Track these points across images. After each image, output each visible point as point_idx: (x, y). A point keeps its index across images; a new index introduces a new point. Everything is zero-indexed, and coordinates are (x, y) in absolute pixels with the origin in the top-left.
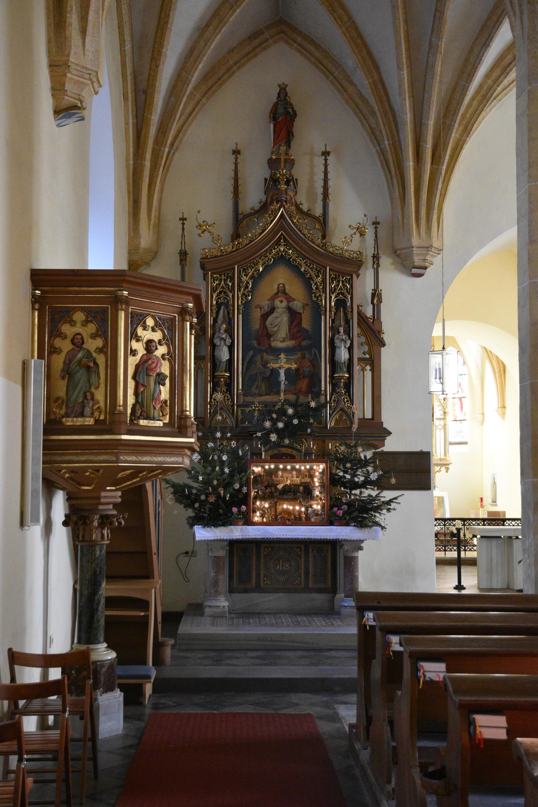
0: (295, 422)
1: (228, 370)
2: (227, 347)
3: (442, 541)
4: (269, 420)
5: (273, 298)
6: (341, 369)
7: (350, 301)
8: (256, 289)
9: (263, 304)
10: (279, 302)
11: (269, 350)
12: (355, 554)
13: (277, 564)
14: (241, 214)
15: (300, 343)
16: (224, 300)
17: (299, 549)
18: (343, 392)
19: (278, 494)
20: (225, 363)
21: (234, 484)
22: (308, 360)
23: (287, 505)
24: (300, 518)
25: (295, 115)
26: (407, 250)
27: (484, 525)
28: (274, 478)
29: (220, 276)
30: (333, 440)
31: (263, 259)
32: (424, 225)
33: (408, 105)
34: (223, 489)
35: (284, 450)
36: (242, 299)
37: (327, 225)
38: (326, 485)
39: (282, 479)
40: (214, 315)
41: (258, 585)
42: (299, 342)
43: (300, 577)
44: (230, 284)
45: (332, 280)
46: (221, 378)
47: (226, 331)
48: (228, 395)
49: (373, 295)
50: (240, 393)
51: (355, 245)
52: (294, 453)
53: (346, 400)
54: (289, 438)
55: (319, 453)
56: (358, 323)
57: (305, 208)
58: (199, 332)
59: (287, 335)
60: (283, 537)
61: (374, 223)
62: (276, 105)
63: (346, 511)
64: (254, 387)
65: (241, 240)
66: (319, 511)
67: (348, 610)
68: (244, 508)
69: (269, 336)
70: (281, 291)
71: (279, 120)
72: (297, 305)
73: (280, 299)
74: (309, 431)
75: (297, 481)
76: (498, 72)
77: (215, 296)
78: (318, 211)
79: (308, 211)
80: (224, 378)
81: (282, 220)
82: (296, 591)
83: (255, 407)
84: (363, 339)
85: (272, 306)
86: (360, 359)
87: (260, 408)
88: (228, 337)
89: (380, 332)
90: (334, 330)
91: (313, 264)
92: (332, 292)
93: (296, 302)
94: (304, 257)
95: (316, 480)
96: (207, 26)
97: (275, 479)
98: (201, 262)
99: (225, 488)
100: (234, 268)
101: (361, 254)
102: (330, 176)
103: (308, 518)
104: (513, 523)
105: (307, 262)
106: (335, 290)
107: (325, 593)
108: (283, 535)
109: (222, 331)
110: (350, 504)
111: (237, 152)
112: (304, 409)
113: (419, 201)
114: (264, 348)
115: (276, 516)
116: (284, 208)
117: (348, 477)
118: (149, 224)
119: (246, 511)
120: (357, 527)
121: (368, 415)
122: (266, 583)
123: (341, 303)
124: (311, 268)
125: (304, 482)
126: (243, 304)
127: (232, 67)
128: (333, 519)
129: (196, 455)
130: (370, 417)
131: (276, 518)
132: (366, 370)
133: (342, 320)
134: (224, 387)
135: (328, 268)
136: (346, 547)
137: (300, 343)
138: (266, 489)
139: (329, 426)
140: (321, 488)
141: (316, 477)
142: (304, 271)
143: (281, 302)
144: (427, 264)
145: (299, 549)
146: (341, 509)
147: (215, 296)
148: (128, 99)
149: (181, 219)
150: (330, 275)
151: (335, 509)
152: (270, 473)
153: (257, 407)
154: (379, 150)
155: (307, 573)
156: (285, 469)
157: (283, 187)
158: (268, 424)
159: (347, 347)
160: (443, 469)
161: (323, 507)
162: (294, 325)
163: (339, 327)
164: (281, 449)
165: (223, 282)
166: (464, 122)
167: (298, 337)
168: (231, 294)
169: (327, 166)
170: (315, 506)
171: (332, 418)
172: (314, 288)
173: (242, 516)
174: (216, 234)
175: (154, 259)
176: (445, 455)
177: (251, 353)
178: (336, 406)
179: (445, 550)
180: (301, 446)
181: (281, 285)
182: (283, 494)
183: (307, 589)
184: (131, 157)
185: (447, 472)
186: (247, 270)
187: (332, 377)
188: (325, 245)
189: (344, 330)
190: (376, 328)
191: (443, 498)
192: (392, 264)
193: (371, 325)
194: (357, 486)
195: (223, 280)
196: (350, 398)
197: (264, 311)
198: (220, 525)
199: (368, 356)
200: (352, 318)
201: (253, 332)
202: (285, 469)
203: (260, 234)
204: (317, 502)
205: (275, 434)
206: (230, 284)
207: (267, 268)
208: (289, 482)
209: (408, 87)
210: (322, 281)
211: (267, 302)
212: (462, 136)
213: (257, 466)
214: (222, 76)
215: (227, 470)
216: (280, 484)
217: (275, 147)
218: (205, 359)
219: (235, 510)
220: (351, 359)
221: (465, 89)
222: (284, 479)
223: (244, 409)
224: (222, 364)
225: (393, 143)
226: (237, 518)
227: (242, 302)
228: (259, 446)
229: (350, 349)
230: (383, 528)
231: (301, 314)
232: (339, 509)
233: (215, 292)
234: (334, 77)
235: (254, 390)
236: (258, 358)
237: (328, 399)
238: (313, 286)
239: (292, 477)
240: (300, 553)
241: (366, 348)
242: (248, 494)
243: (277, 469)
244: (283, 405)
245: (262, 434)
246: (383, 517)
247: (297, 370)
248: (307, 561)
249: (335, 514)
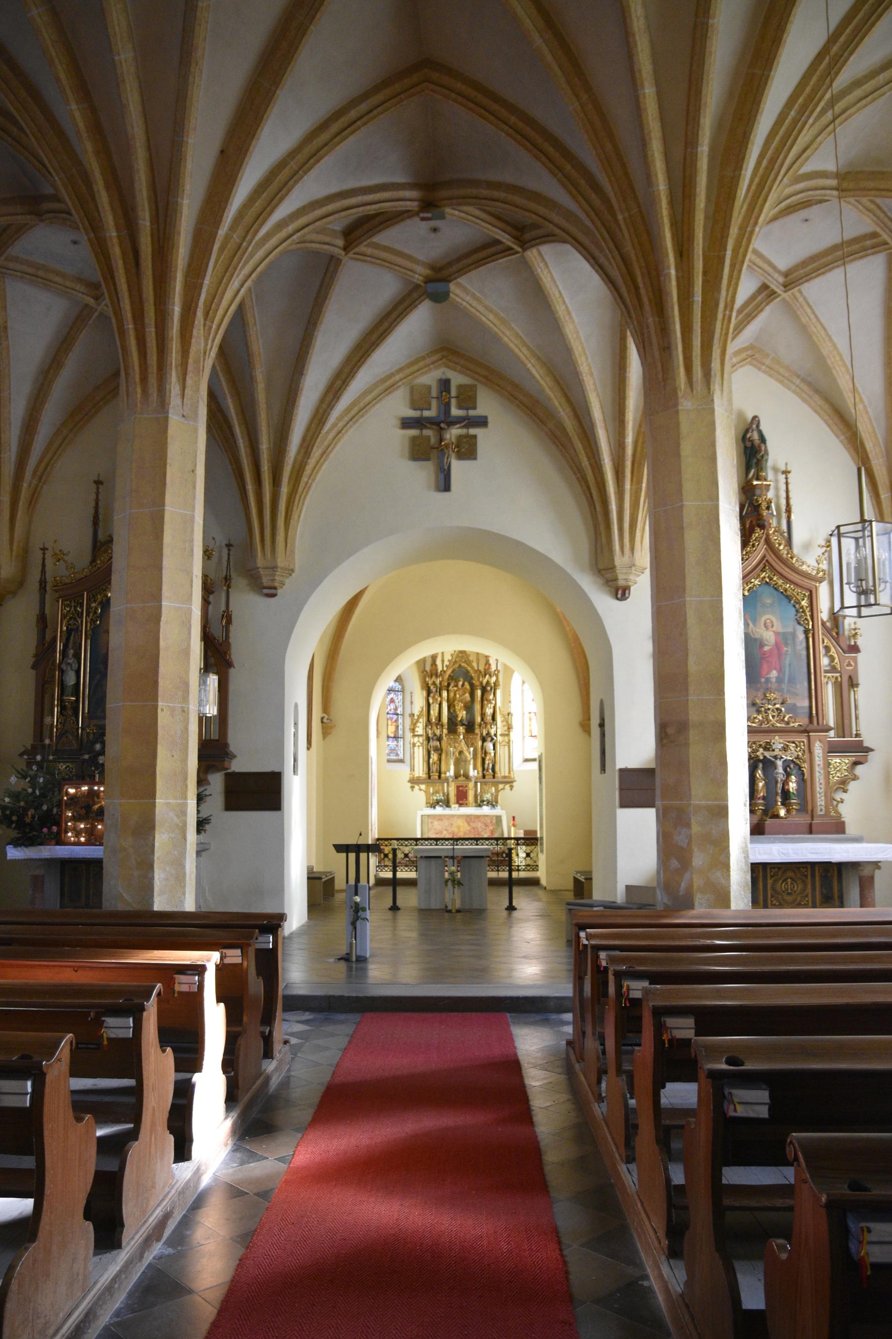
3: (494, 861)
27: (437, 845)
29: (71, 602)
36: (91, 624)
60: (88, 857)
61: (41, 549)
68: (55, 829)
76: (330, 396)
96: (50, 368)
111: (98, 483)
118: (11, 555)
144: (276, 584)
149: (41, 549)
160: (507, 787)
165: (73, 609)
176: (509, 773)
177: (98, 677)
179: (498, 871)
185: (511, 789)
191: (500, 816)
209: (237, 414)
212: (304, 458)
213: (72, 788)
215: (38, 793)
233: (65, 618)
242: (60, 815)
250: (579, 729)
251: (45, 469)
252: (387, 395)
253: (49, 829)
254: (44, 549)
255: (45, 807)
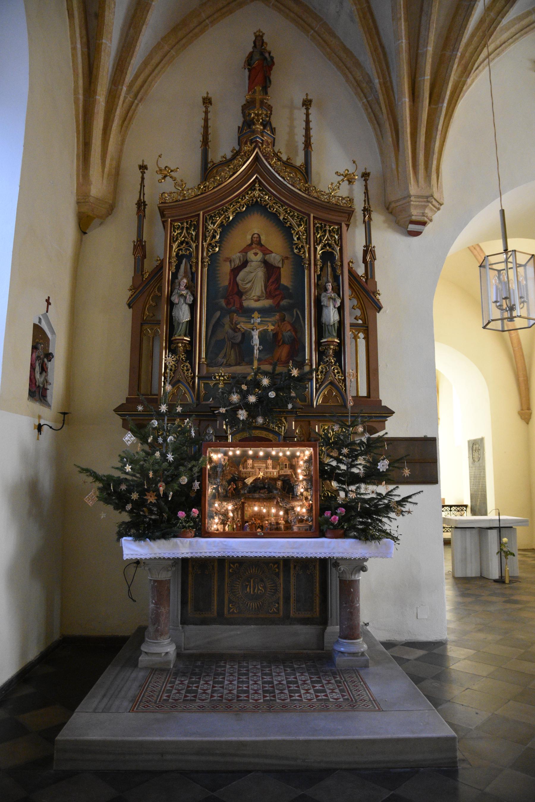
0: (272, 394)
1: (189, 334)
2: (187, 305)
4: (237, 392)
5: (245, 251)
6: (329, 333)
7: (338, 253)
8: (225, 239)
9: (234, 257)
10: (253, 255)
11: (240, 311)
12: (356, 577)
13: (247, 585)
14: (210, 162)
15: (279, 303)
16: (186, 252)
17: (276, 566)
18: (333, 361)
19: (246, 492)
20: (184, 326)
21: (181, 477)
22: (289, 322)
23: (259, 506)
24: (278, 529)
25: (273, 64)
26: (404, 201)
28: (241, 469)
30: (320, 421)
31: (234, 206)
32: (423, 171)
33: (403, 28)
34: (164, 484)
35: (257, 433)
37: (309, 174)
38: (314, 479)
39: (252, 470)
40: (173, 269)
41: (221, 614)
42: (277, 302)
43: (278, 603)
44: (194, 233)
45: (317, 230)
46: (178, 343)
47: (187, 287)
48: (187, 364)
49: (365, 253)
50: (203, 362)
51: (343, 191)
52: (271, 436)
53: (336, 371)
54: (264, 416)
55: (302, 439)
56: (349, 284)
57: (284, 158)
58: (157, 292)
59: (262, 292)
60: (252, 555)
62: (251, 56)
63: (343, 516)
64: (222, 355)
65: (208, 183)
66: (304, 516)
67: (345, 658)
69: (240, 294)
70: (256, 242)
71: (254, 66)
72: (275, 258)
73: (254, 251)
74: (290, 406)
75: (274, 474)
77: (175, 246)
78: (299, 161)
79: (288, 159)
80: (182, 343)
81: (257, 163)
82: (272, 622)
83: (220, 377)
84: (355, 302)
85: (245, 260)
86: (352, 325)
87: (226, 377)
88: (189, 294)
89: (375, 292)
90: (321, 288)
91: (294, 212)
92: (318, 242)
93: (273, 254)
94: (284, 204)
95: (299, 471)
97: (243, 470)
98: (159, 207)
99: (167, 483)
100: (199, 214)
101: (351, 200)
102: (312, 125)
103: (288, 525)
104: (458, 509)
105: (287, 208)
106: (321, 241)
107: (311, 624)
108: (251, 552)
109: (182, 287)
110: (349, 506)
112: (283, 379)
113: (416, 142)
114: (233, 308)
115: (244, 522)
116: (260, 149)
117: (343, 467)
118: (103, 172)
119: (198, 517)
120: (360, 539)
121: (363, 392)
122: (231, 611)
123: (328, 257)
124: (291, 216)
125: (283, 475)
126: (209, 257)
127: (205, 20)
128: (325, 527)
129: (129, 435)
130: (365, 394)
131: (242, 527)
132: (359, 338)
133: (329, 275)
134: (183, 355)
135: (312, 215)
136: (342, 568)
137: (279, 303)
138: (229, 484)
139: (315, 403)
140: (307, 483)
141: (300, 467)
142: (284, 218)
143: (256, 254)
144: (426, 219)
145: (276, 566)
146: (336, 514)
147: (175, 246)
148: (73, 17)
150: (314, 224)
151: (328, 514)
152: (236, 462)
153: (221, 376)
154: (366, 103)
155: (287, 599)
156: (255, 457)
157: (260, 127)
158: (235, 398)
159: (337, 306)
161: (310, 511)
162: (271, 281)
163: (326, 283)
164: (254, 431)
165: (185, 231)
166: (463, 62)
167: (276, 295)
168: (195, 245)
169: (309, 115)
170: (298, 509)
171: (319, 393)
172: (296, 239)
173: (192, 524)
174: (178, 180)
175: (110, 214)
177: (218, 314)
178: (324, 379)
180: (279, 427)
181: (256, 236)
182: (255, 492)
183: (287, 620)
184: (81, 91)
186: (215, 217)
187: (319, 344)
188: (308, 189)
189: (332, 287)
190: (369, 287)
192: (385, 222)
193: (365, 284)
194: (355, 479)
195: (185, 228)
196: (341, 368)
197: (235, 266)
198: (159, 538)
199: (360, 322)
200: (342, 273)
201: (221, 289)
202: (255, 457)
203: (231, 177)
204: (301, 503)
205: (244, 411)
206: (194, 233)
207: (239, 216)
208: (261, 474)
210: (304, 230)
211: (239, 254)
213: (216, 452)
214: (193, 29)
215: (170, 457)
216: (249, 477)
217: (250, 93)
218: (160, 324)
219: (181, 514)
220: (341, 322)
221: (463, 27)
222: (255, 470)
223: (207, 382)
224: (180, 327)
225: (385, 83)
226: (184, 527)
227: (207, 254)
228: (225, 427)
229: (341, 310)
230: (395, 539)
231: (279, 268)
232: (334, 513)
233: (174, 242)
234: (315, 31)
235: (220, 359)
236: (226, 320)
237: (314, 367)
238: (294, 237)
239: (267, 468)
240: (277, 570)
241: (358, 313)
242: (202, 491)
243: (244, 456)
244: (256, 374)
245: (226, 410)
246: (394, 524)
247: (275, 335)
248: (287, 582)
249: (327, 521)
250: (517, 418)
251: (142, 86)
252: (522, 35)
253: (188, 513)
254: (143, 168)
255: (184, 480)
